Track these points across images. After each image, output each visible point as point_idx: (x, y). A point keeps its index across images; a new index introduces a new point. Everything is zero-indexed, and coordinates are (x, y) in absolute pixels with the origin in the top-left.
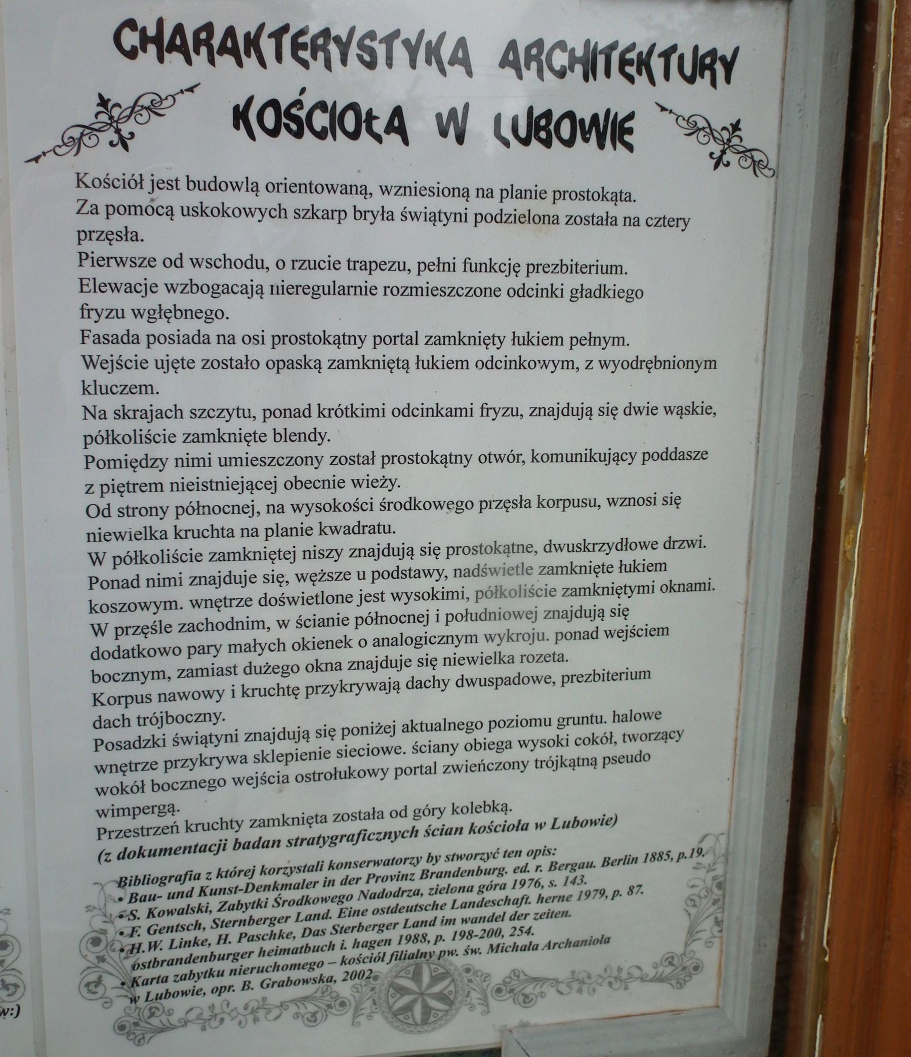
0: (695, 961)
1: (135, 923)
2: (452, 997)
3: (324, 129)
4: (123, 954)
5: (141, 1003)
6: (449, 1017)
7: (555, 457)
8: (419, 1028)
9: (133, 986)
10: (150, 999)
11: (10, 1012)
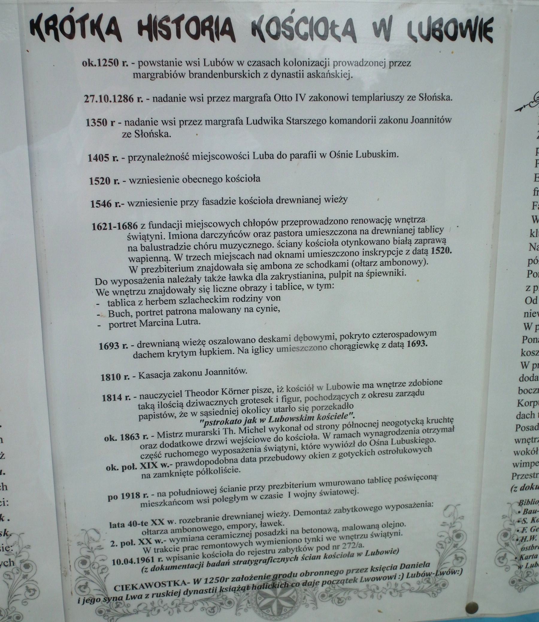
0: (17, 613)
1: (525, 525)
2: (295, 600)
3: (306, 34)
4: (518, 542)
5: (523, 569)
6: (293, 611)
8: (276, 618)
9: (520, 560)
10: (528, 567)
11: (458, 572)
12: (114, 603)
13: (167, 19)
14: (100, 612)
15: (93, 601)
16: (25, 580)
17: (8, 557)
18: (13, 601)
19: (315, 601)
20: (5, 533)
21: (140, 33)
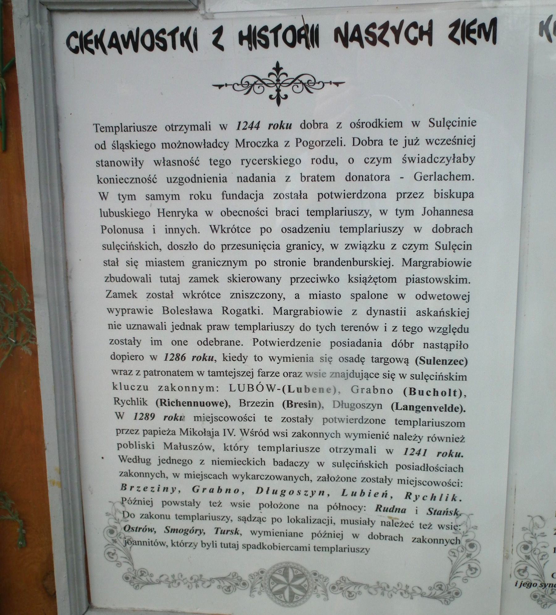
7: (391, 279)
8: (288, 604)
12: (549, 590)
13: (163, 31)
14: (535, 596)
15: (529, 585)
16: (469, 558)
17: (456, 536)
18: (455, 577)
19: (325, 591)
20: (456, 513)
21: (241, 43)
